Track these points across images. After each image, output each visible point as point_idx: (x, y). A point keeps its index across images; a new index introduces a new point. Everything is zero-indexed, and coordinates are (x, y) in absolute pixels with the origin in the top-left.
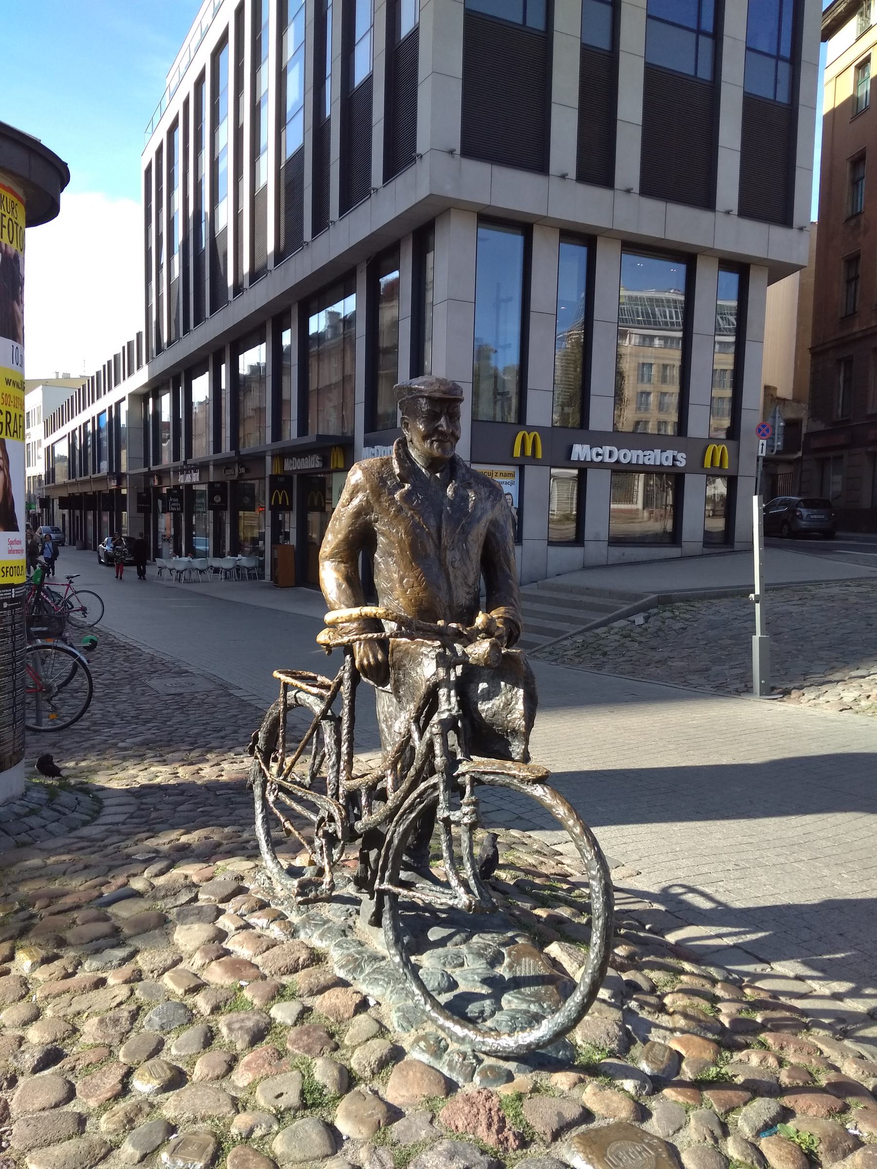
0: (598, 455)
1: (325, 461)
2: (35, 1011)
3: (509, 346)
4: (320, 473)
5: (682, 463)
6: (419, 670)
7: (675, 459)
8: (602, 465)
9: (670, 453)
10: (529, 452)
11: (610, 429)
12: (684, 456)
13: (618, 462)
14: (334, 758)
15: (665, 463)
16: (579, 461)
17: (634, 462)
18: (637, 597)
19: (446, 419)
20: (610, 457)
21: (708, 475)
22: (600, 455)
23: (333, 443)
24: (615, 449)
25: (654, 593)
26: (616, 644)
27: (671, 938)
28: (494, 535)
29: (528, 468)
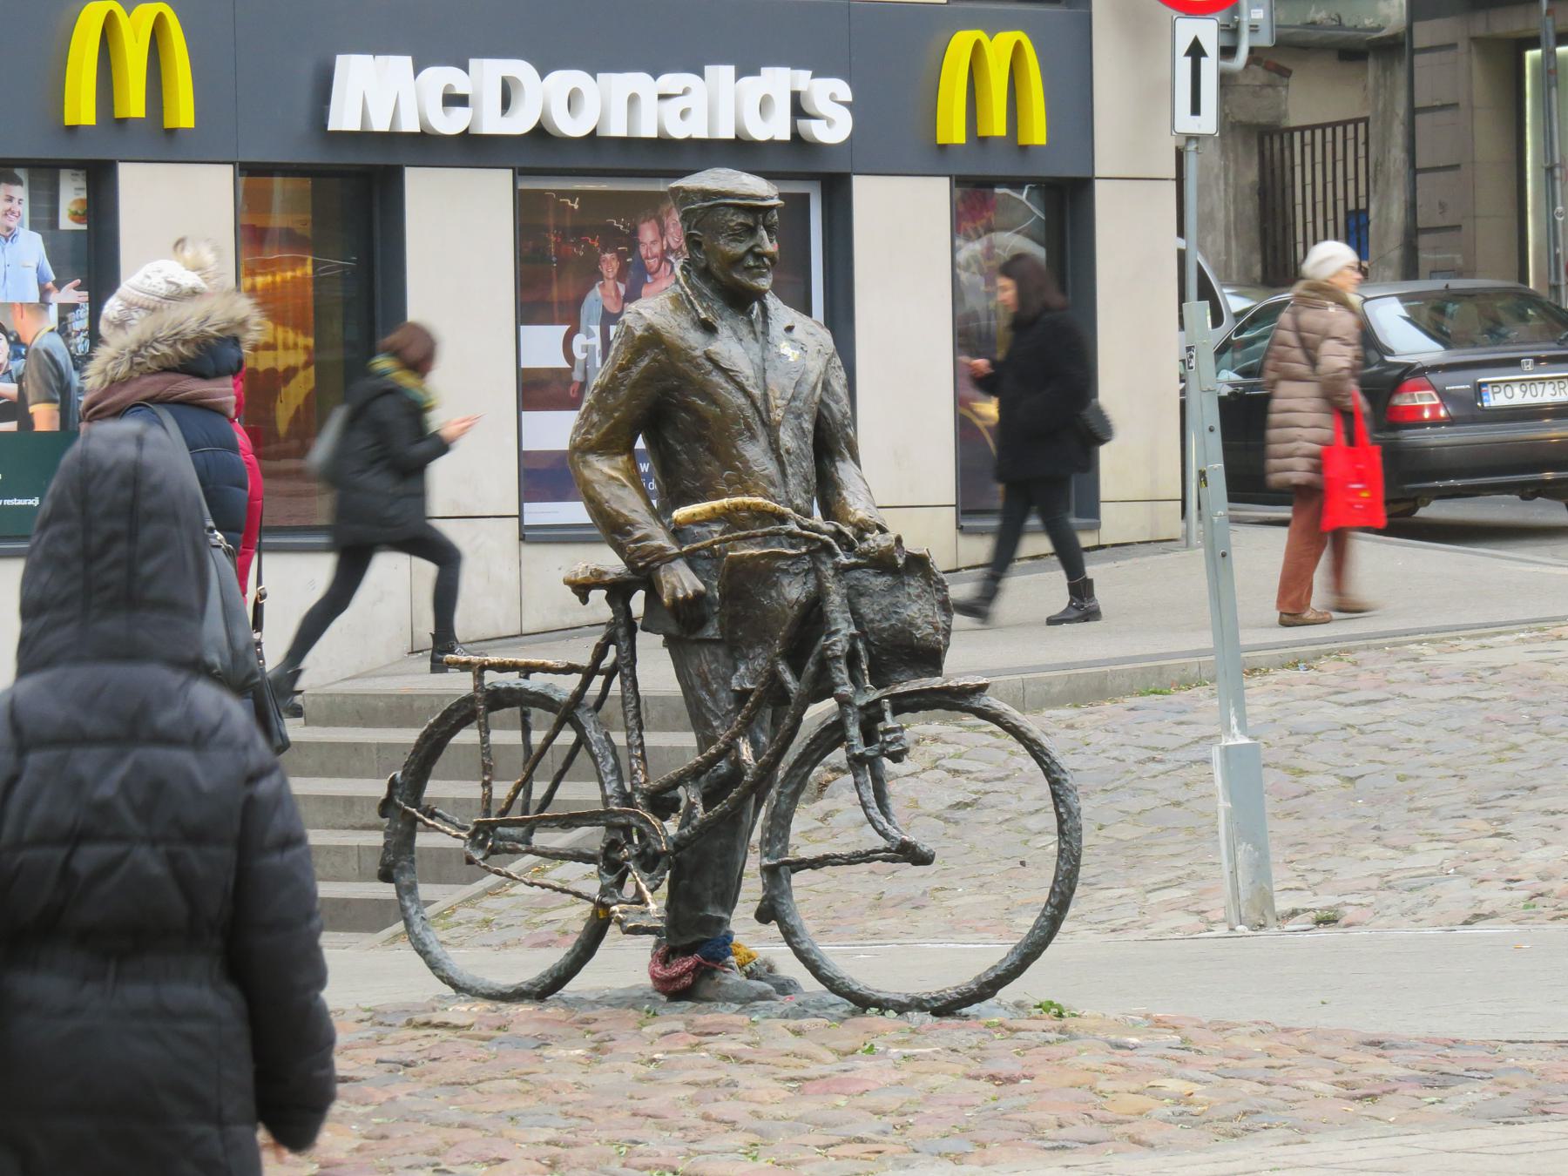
0: (454, 100)
5: (833, 125)
6: (774, 594)
7: (799, 109)
8: (473, 150)
9: (779, 81)
10: (134, 104)
11: (787, 136)
12: (843, 90)
13: (541, 134)
14: (611, 760)
16: (363, 138)
17: (617, 129)
20: (506, 104)
21: (959, 182)
24: (521, 69)
28: (827, 406)
29: (130, 177)
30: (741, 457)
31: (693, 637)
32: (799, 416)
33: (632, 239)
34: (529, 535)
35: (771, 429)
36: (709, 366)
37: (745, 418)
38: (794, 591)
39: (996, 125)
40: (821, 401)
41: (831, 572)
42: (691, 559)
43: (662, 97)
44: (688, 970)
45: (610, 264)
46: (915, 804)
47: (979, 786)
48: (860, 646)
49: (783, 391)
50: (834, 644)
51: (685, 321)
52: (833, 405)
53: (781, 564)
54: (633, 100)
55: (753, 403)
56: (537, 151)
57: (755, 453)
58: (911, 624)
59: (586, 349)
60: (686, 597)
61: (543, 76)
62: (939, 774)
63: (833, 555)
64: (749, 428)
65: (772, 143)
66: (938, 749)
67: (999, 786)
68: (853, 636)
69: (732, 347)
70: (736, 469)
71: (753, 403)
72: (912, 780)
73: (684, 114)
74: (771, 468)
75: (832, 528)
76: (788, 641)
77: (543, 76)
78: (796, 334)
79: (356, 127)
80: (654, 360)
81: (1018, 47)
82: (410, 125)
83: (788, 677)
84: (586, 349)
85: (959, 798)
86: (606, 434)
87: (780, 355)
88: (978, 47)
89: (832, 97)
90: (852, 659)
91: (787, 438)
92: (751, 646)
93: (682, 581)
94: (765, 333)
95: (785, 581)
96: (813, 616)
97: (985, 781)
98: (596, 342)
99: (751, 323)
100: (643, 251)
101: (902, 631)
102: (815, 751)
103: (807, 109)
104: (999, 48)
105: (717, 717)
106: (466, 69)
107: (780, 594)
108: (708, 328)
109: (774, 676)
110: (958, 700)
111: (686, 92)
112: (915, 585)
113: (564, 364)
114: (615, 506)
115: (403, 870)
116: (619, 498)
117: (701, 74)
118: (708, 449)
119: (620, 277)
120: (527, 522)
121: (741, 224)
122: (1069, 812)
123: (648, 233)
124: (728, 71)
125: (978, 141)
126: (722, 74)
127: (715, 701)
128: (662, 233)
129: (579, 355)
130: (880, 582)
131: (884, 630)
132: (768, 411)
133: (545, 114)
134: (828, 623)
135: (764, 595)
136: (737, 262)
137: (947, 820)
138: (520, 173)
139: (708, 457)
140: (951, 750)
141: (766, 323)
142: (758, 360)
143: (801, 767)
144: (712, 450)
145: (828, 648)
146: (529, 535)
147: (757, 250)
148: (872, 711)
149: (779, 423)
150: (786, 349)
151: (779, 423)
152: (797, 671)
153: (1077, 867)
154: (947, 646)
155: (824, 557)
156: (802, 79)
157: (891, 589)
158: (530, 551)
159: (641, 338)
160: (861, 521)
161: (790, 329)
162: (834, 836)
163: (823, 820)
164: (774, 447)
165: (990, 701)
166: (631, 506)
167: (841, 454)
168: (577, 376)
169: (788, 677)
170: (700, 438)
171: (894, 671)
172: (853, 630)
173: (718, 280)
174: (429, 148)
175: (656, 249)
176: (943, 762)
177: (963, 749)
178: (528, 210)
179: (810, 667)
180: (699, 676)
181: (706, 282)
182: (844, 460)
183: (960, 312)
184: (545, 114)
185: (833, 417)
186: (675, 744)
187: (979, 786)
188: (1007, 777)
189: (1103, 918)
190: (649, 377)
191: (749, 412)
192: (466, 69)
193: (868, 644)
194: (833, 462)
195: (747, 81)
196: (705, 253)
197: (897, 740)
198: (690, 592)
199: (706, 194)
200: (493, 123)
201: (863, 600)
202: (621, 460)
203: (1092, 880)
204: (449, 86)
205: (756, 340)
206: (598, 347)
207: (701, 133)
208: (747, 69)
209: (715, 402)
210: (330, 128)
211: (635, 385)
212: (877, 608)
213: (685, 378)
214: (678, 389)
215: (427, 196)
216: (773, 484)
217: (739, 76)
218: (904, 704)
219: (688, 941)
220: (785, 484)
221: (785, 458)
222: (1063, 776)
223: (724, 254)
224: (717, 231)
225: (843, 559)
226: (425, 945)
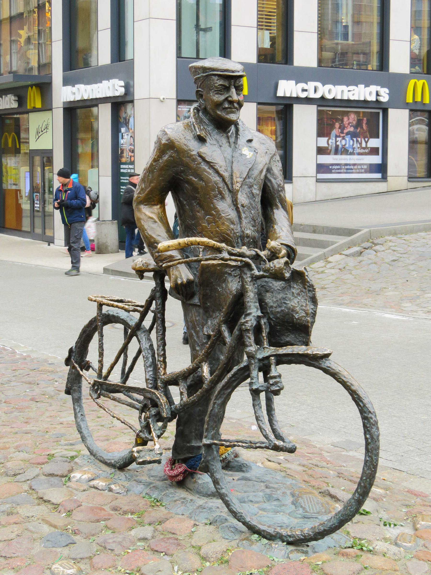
0: (304, 90)
1: (21, 101)
2: (345, 51)
3: (210, 29)
4: (17, 113)
5: (385, 98)
7: (378, 94)
8: (308, 101)
9: (374, 88)
12: (387, 91)
13: (323, 98)
15: (369, 99)
16: (284, 98)
17: (339, 97)
18: (349, 232)
19: (172, 193)
20: (315, 91)
21: (411, 110)
22: (306, 90)
23: (29, 83)
25: (366, 227)
26: (333, 278)
27: (172, 229)
28: (270, 181)
30: (215, 208)
31: (188, 302)
32: (251, 187)
33: (342, 121)
34: (318, 181)
35: (234, 193)
36: (199, 159)
37: (218, 188)
38: (233, 285)
39: (419, 99)
40: (266, 177)
41: (249, 279)
42: (189, 264)
43: (349, 91)
44: (181, 473)
45: (337, 125)
46: (383, 259)
47: (399, 255)
48: (263, 322)
49: (241, 173)
50: (247, 322)
51: (189, 136)
52: (273, 180)
53: (227, 270)
54: (342, 91)
55: (224, 180)
56: (322, 101)
57: (224, 207)
58: (293, 310)
59: (332, 142)
60: (182, 283)
61: (323, 86)
62: (390, 251)
63: (251, 269)
64: (220, 193)
65: (372, 101)
66: (391, 244)
67: (404, 256)
68: (259, 317)
69: (215, 151)
70: (212, 215)
71: (224, 180)
72: (383, 253)
73: (353, 95)
74: (233, 214)
75: (254, 253)
76: (227, 315)
77: (323, 86)
78: (253, 144)
79: (283, 95)
80: (171, 156)
81: (424, 83)
82: (294, 95)
83: (226, 334)
84: (332, 142)
85: (394, 258)
86: (147, 195)
87: (241, 155)
88: (415, 83)
89: (385, 92)
90: (258, 329)
91: (242, 198)
92: (214, 311)
93: (184, 274)
94: (235, 143)
95: (230, 279)
96: (238, 305)
97: (401, 254)
98: (334, 141)
99: (228, 138)
100: (344, 123)
101: (288, 314)
102: (234, 381)
103: (379, 94)
104: (420, 83)
105: (199, 346)
106: (307, 84)
107: (227, 286)
108: (201, 140)
109: (219, 334)
110: (314, 361)
111: (354, 90)
112: (296, 288)
113: (327, 146)
114: (150, 233)
115: (75, 390)
116: (152, 228)
117: (357, 86)
118: (198, 204)
119: (340, 128)
120: (318, 178)
121: (221, 85)
122: (372, 438)
123: (345, 119)
124: (363, 86)
125: (415, 102)
126: (362, 86)
127: (198, 337)
128: (349, 119)
129: (330, 144)
130: (277, 285)
131: (278, 312)
132: (232, 184)
133: (324, 93)
134: (246, 308)
135: (219, 286)
136: (219, 105)
137: (390, 265)
138: (319, 106)
139: (198, 208)
140: (393, 244)
141: (237, 138)
142: (229, 157)
143: (226, 389)
144: (201, 206)
145: (243, 324)
146: (318, 181)
147: (230, 99)
148: (266, 362)
149: (238, 191)
150: (246, 152)
151: (238, 191)
152: (231, 331)
153: (375, 472)
154: (313, 323)
155: (246, 270)
156: (378, 88)
157: (284, 289)
158: (319, 184)
159: (165, 144)
160: (272, 247)
161: (250, 141)
162: (361, 268)
163: (359, 263)
164: (235, 203)
165: (330, 363)
166: (158, 233)
167: (276, 205)
168: (330, 148)
169: (226, 334)
170: (195, 198)
171: (283, 335)
172: (259, 313)
173: (211, 115)
174: (298, 100)
175: (347, 123)
176: (391, 248)
177: (397, 244)
178: (319, 113)
179: (236, 332)
180: (191, 322)
181: (206, 116)
182: (278, 208)
184: (324, 93)
185: (273, 187)
186: (179, 359)
187: (399, 255)
188: (406, 253)
189: (426, 305)
190: (169, 165)
191: (221, 185)
192: (307, 84)
193: (269, 319)
194: (272, 209)
195: (366, 88)
196: (204, 100)
197: (276, 383)
198: (185, 280)
199: (204, 69)
200: (312, 95)
201: (268, 295)
202: (157, 208)
203: (424, 289)
204: (303, 87)
205: (230, 146)
206: (334, 142)
207: (356, 98)
208: (367, 86)
209: (201, 179)
210: (278, 95)
211: (161, 169)
212: (275, 300)
213: (187, 166)
214: (183, 171)
215: (297, 109)
216: (233, 223)
217: (365, 87)
218: (282, 360)
219: (182, 457)
220: (241, 223)
221: (241, 209)
222: (370, 415)
223: (212, 101)
224: (210, 88)
225: (256, 272)
226: (81, 429)
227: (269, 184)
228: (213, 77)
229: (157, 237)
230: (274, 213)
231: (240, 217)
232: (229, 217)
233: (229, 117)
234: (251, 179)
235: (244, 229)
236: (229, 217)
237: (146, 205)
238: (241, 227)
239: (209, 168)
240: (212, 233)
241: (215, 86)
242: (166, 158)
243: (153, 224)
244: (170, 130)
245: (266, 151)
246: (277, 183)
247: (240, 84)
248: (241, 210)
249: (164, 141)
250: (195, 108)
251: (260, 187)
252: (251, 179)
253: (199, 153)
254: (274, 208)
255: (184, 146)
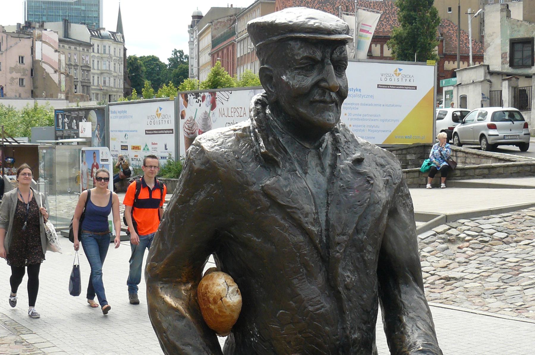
28: (394, 232)
36: (265, 202)
64: (305, 265)
74: (326, 305)
91: (347, 275)
99: (320, 157)
121: (307, 58)
136: (302, 95)
147: (323, 84)
159: (199, 171)
182: (407, 283)
183: (514, 113)
205: (323, 171)
227: (392, 238)
228: (290, 42)
229: (184, 347)
230: (400, 292)
231: (341, 311)
232: (323, 310)
233: (321, 118)
234: (362, 234)
235: (350, 332)
236: (323, 310)
237: (166, 282)
238: (343, 328)
239: (283, 218)
240: (289, 343)
241: (295, 60)
242: (201, 196)
243: (179, 320)
244: (210, 143)
245: (387, 178)
246: (405, 237)
247: (342, 56)
248: (344, 296)
249: (197, 166)
250: (259, 100)
251: (378, 251)
252: (362, 234)
253: (265, 188)
254: (400, 281)
255: (237, 176)
